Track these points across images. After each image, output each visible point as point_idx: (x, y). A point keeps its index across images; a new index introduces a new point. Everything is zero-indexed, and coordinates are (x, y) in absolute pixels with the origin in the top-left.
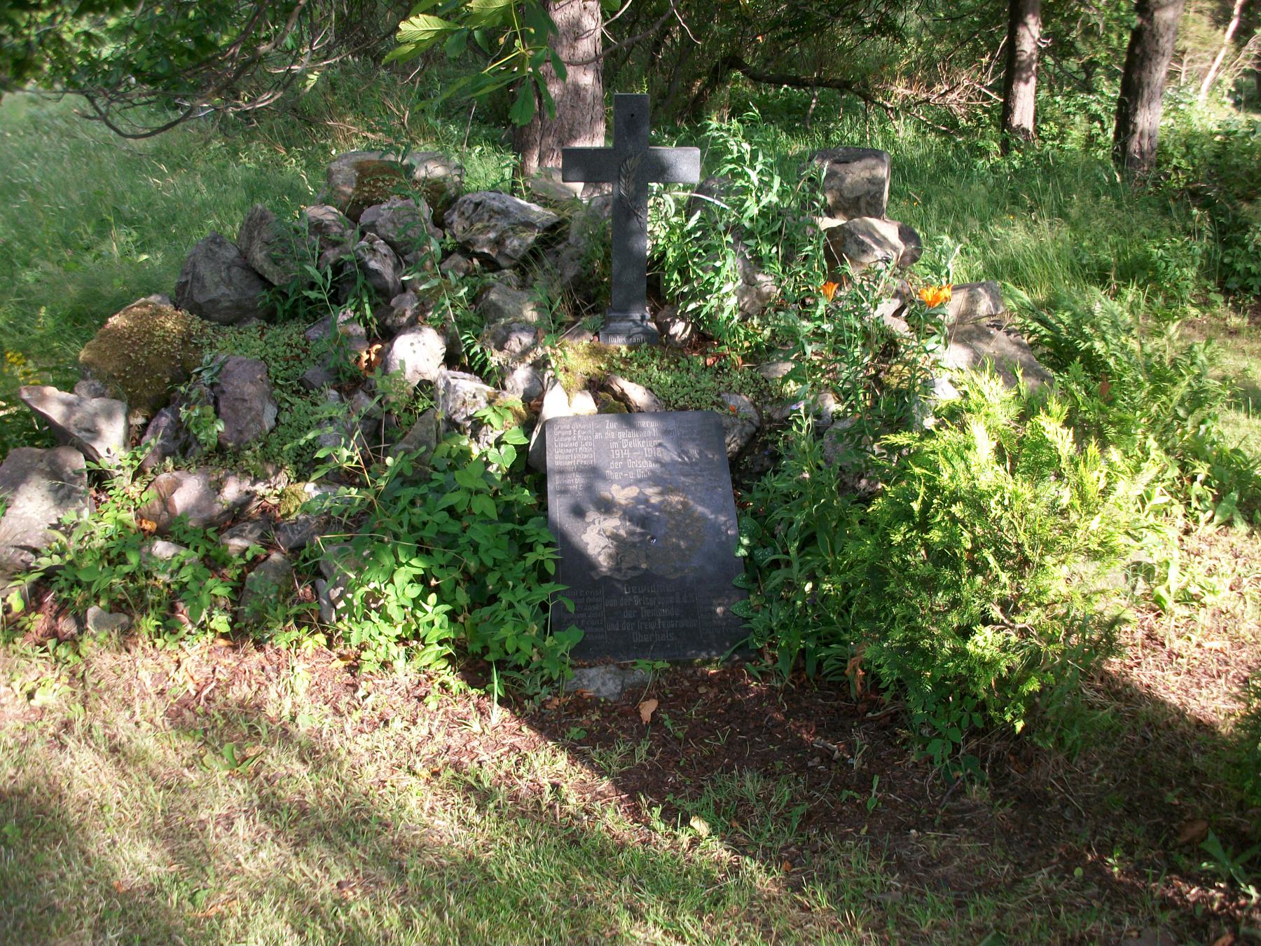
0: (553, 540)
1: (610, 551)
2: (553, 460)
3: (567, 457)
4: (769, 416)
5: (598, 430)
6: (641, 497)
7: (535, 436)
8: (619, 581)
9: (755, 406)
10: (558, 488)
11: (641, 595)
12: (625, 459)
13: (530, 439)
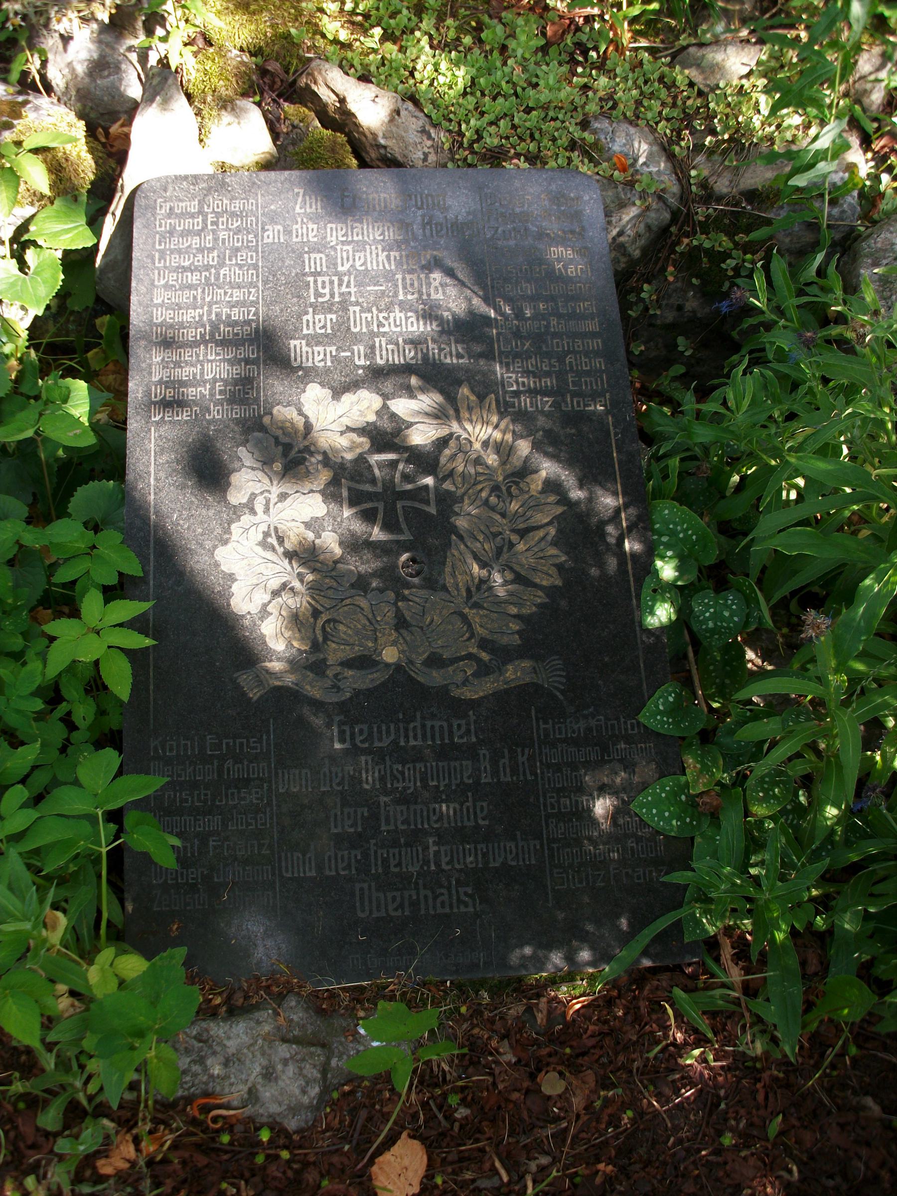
0: (133, 568)
1: (293, 602)
2: (148, 306)
3: (185, 297)
4: (704, 184)
5: (273, 218)
6: (386, 425)
7: (109, 226)
8: (317, 705)
9: (671, 157)
10: (158, 393)
11: (380, 756)
12: (344, 305)
13: (98, 234)
